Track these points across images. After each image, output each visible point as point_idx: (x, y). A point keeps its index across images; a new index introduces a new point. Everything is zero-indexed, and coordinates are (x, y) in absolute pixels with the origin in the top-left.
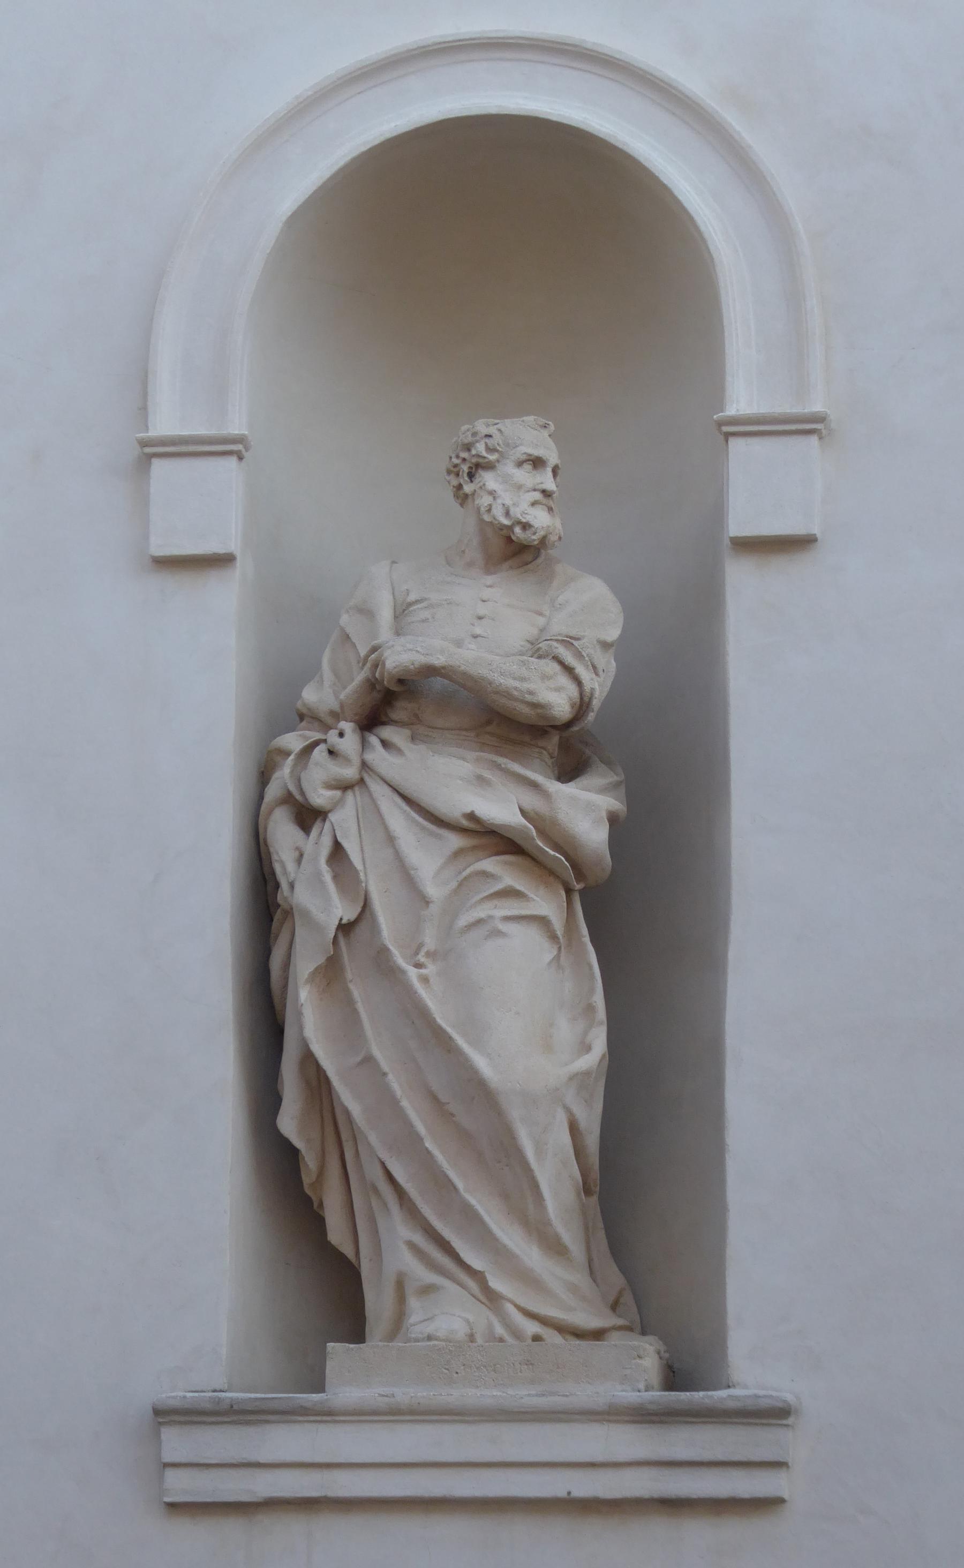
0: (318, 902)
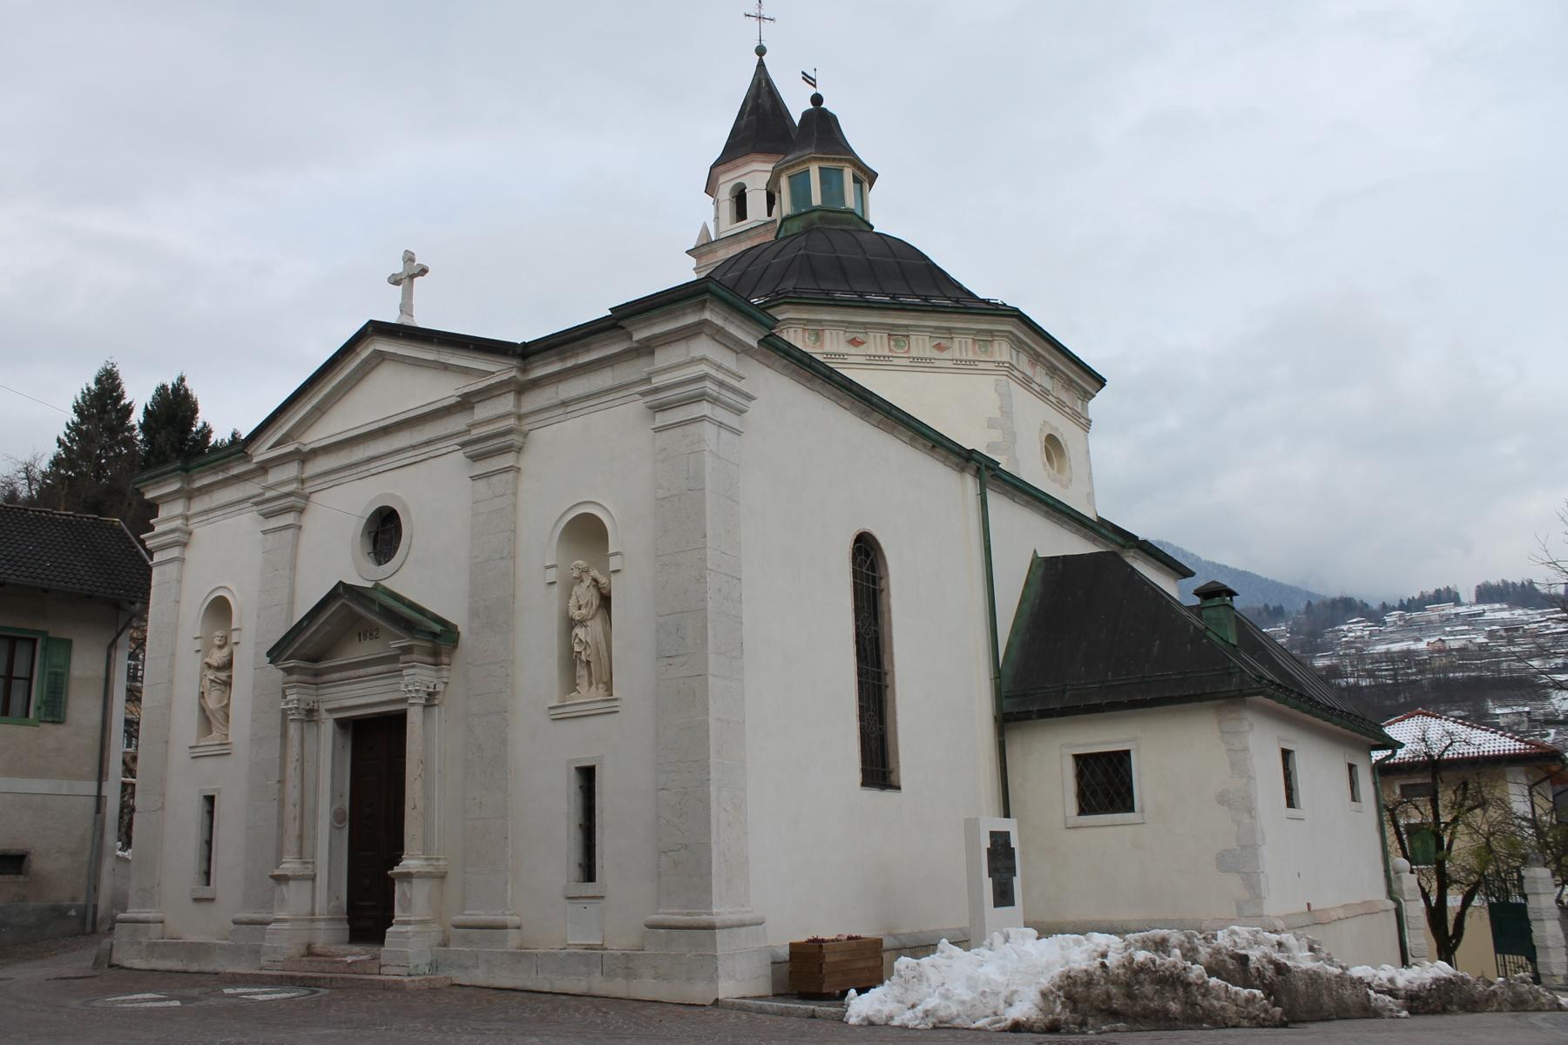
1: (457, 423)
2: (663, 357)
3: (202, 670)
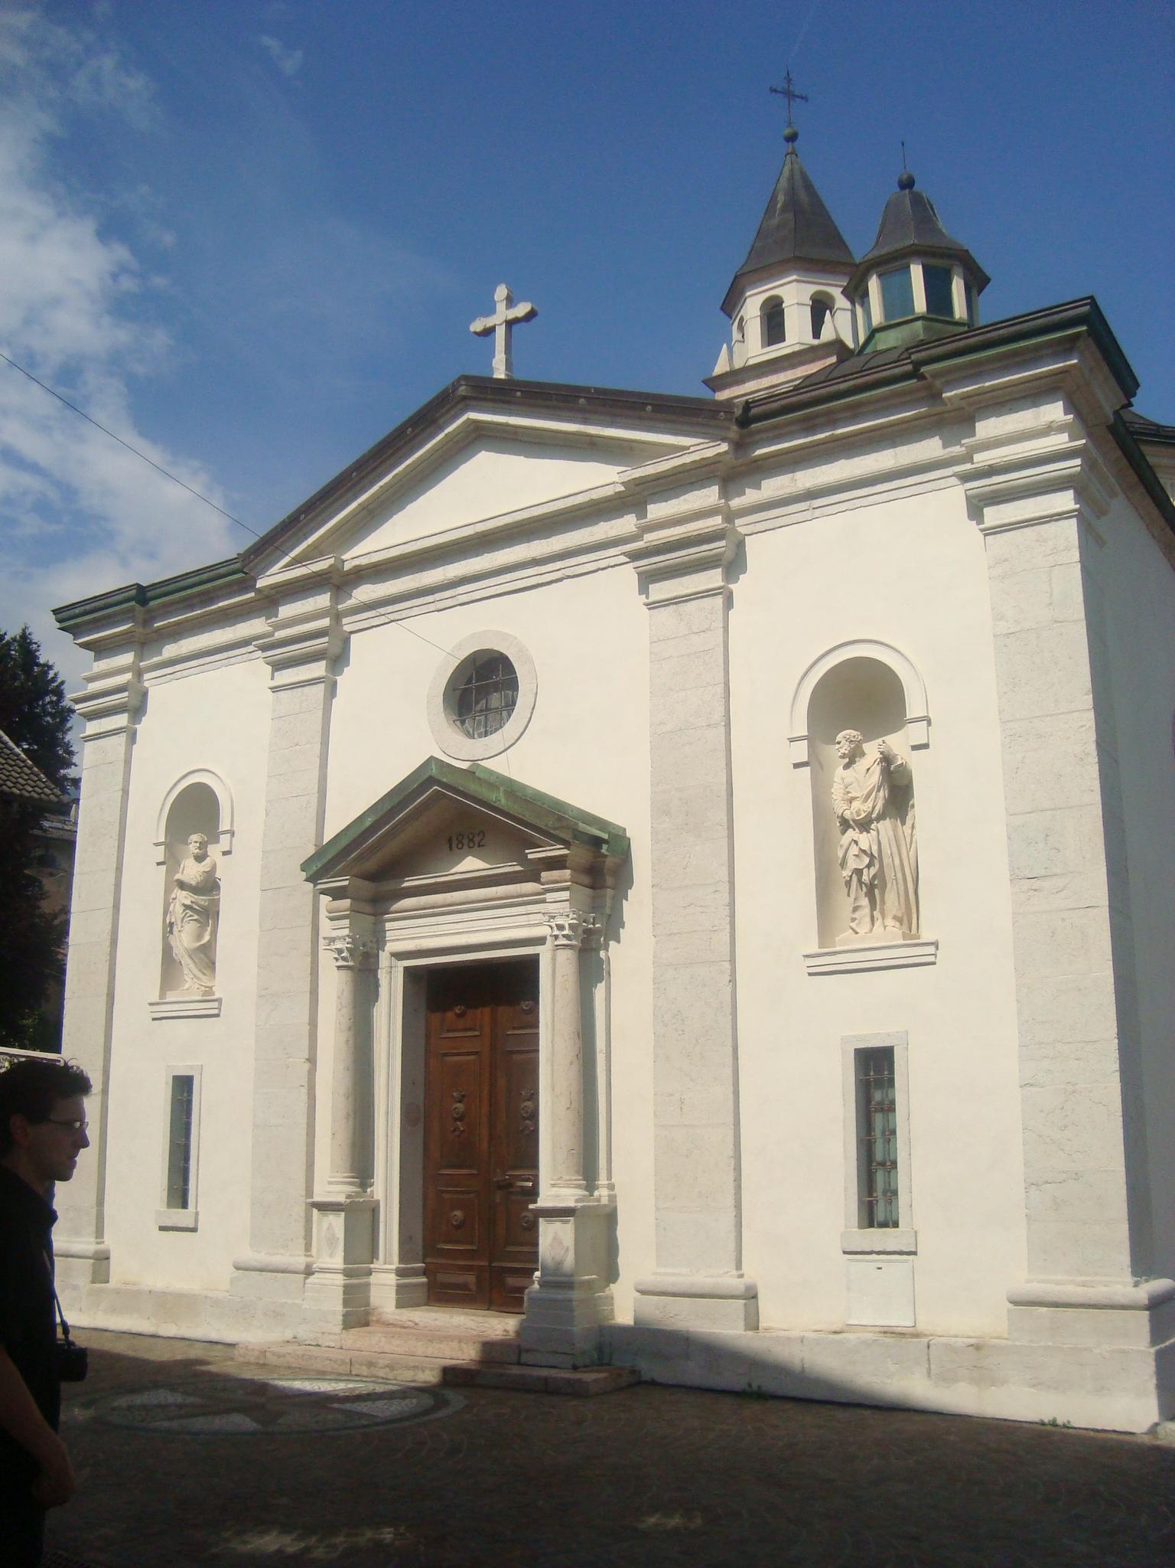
1: (627, 524)
2: (988, 428)
3: (168, 891)
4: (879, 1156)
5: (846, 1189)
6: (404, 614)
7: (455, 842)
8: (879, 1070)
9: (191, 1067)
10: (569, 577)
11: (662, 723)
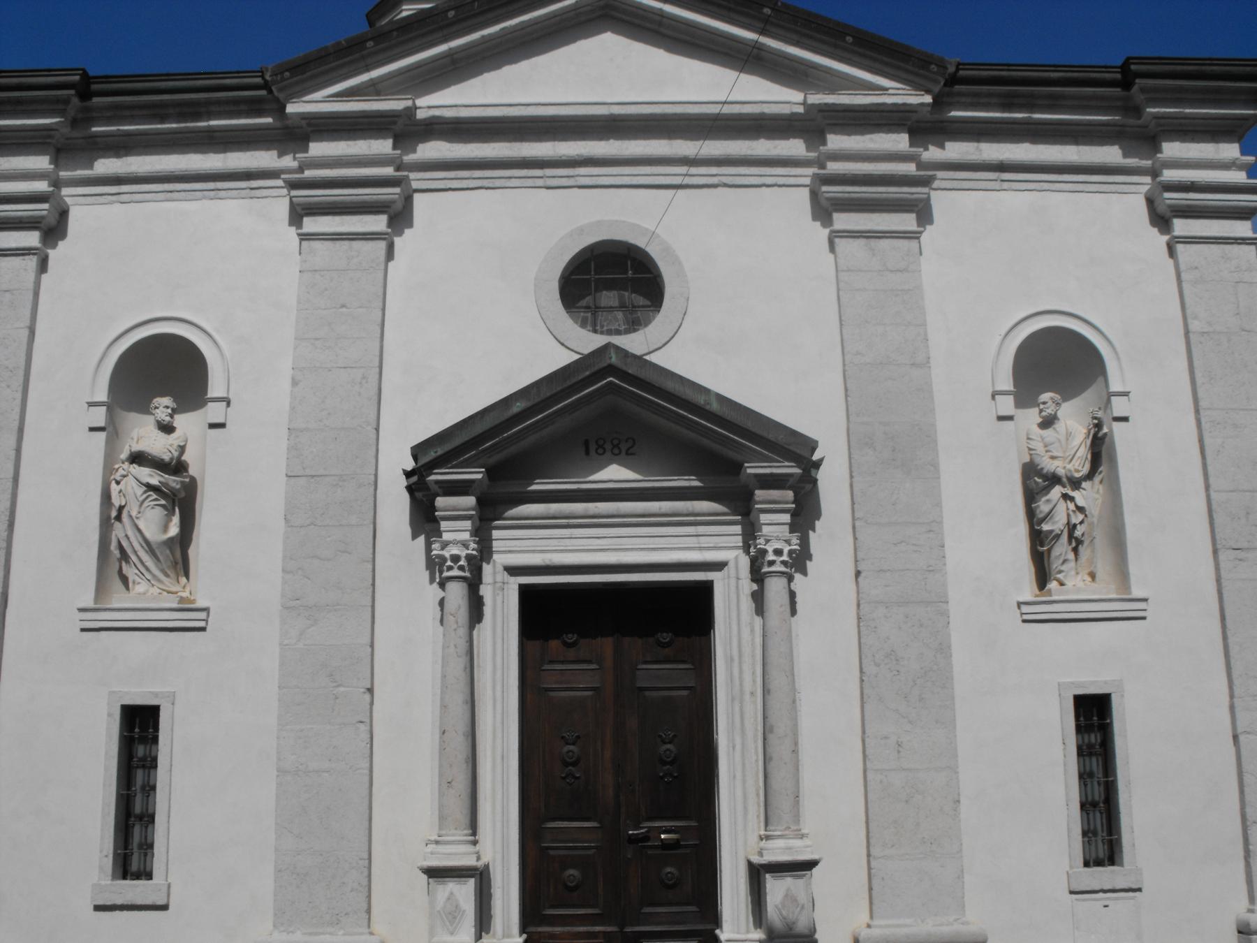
0: (117, 501)
4: (138, 809)
5: (1069, 830)
6: (498, 183)
7: (593, 447)
8: (144, 729)
9: (156, 695)
10: (780, 186)
11: (858, 353)
